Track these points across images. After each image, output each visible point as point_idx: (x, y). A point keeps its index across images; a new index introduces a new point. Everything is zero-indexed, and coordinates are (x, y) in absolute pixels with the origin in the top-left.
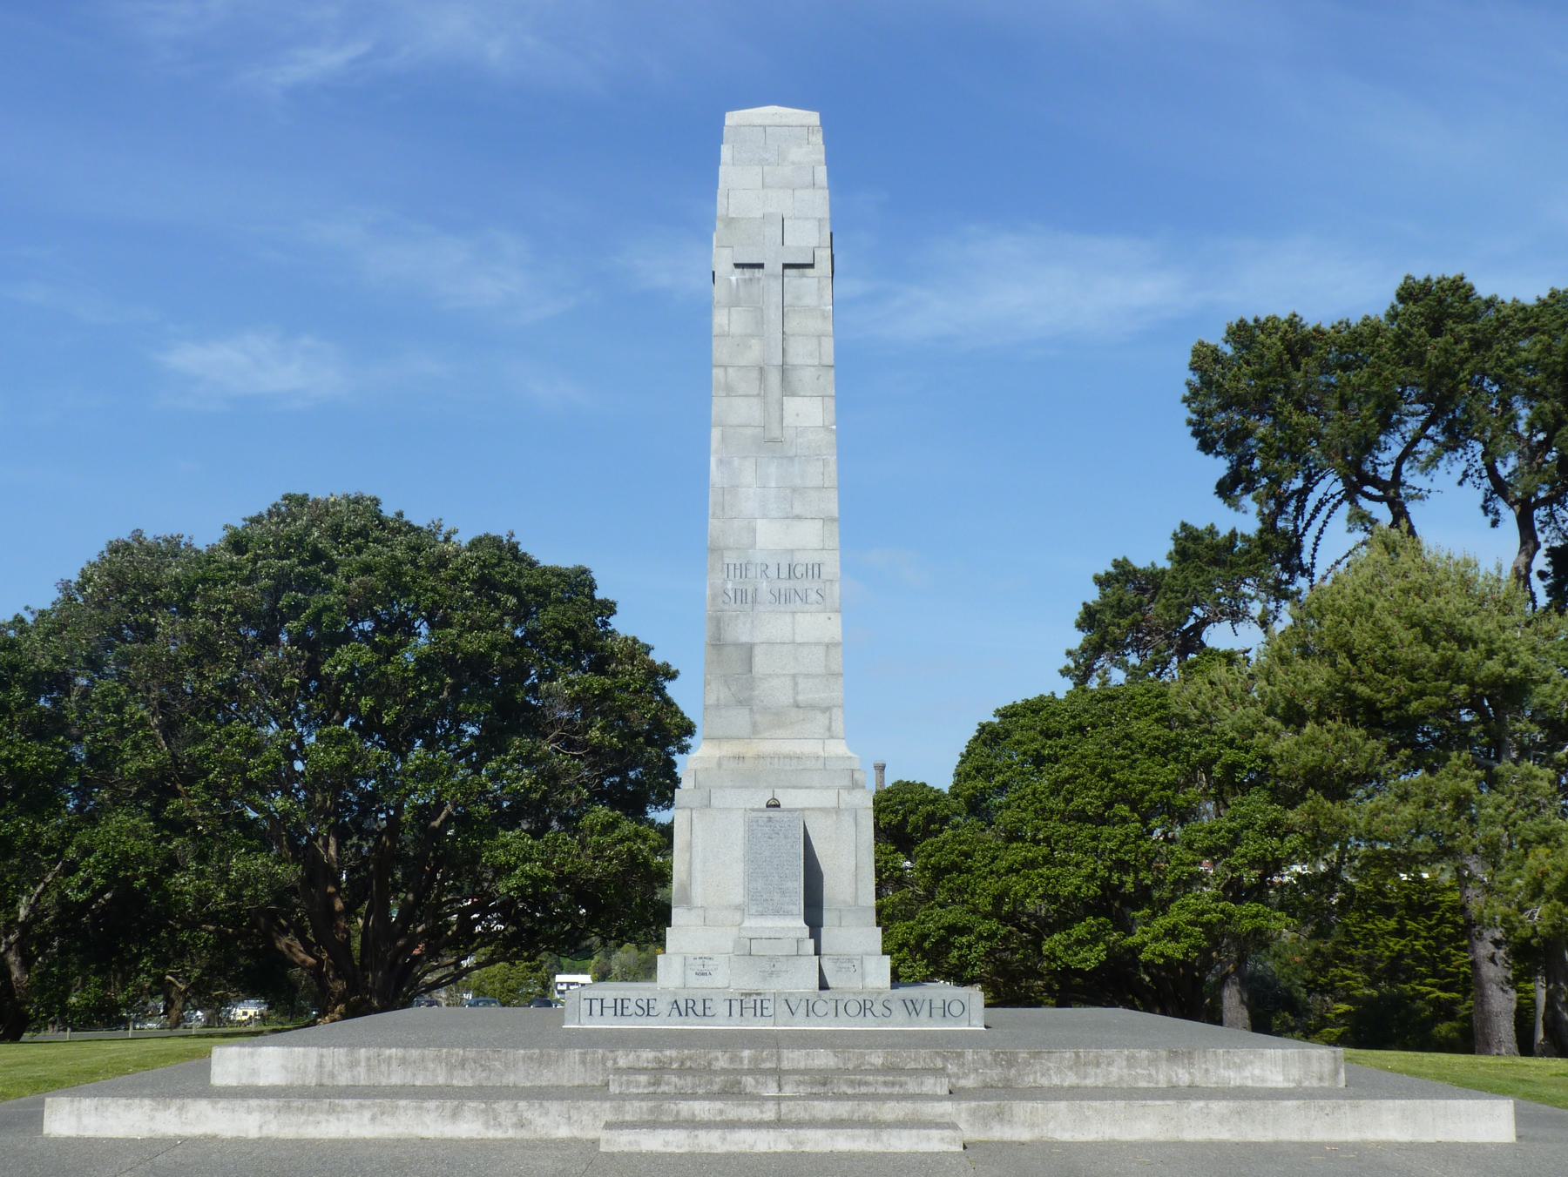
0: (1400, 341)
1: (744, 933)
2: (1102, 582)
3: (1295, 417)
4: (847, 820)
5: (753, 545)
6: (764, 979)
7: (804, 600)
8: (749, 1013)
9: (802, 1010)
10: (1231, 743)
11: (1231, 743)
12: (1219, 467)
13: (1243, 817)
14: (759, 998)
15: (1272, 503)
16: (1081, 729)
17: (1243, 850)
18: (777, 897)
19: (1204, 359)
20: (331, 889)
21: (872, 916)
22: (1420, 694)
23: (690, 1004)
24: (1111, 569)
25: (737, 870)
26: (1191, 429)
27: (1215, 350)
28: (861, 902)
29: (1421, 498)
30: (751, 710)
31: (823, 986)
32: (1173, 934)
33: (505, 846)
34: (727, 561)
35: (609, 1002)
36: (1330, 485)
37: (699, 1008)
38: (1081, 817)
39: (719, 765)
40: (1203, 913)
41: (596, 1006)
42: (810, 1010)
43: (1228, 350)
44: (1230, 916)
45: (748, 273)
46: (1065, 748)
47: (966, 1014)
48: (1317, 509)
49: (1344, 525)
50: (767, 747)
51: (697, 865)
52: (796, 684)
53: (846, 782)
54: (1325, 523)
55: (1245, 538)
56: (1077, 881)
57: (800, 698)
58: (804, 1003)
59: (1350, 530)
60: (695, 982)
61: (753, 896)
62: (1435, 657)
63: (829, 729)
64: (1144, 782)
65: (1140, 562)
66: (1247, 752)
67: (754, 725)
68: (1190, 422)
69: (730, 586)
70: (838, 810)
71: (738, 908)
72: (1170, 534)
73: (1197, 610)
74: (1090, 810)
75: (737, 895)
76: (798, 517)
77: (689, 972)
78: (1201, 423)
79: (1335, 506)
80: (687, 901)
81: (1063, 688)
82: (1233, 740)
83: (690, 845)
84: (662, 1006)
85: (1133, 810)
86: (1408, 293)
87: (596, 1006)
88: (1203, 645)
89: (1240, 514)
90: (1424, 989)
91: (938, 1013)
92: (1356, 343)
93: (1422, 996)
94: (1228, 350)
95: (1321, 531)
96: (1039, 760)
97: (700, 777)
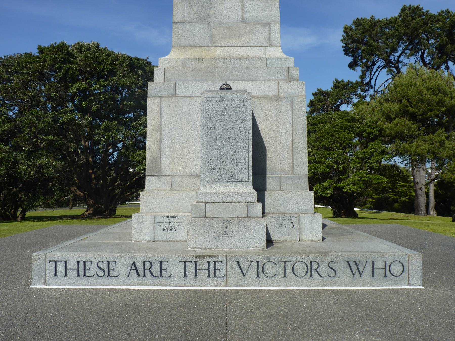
0: (403, 21)
1: (200, 198)
2: (315, 95)
3: (373, 43)
4: (285, 106)
6: (218, 239)
8: (203, 274)
9: (253, 271)
10: (369, 127)
11: (369, 127)
12: (350, 59)
13: (374, 148)
14: (212, 260)
15: (365, 68)
17: (374, 158)
18: (229, 166)
19: (347, 30)
20: (91, 171)
21: (305, 182)
22: (431, 110)
23: (148, 266)
24: (317, 91)
25: (197, 146)
26: (343, 49)
27: (350, 27)
28: (297, 171)
30: (209, 24)
31: (270, 242)
32: (354, 184)
33: (138, 155)
35: (72, 264)
36: (381, 63)
37: (156, 270)
38: (324, 148)
39: (184, 64)
40: (363, 177)
41: (61, 268)
42: (260, 271)
43: (353, 27)
44: (370, 179)
47: (405, 273)
48: (377, 70)
49: (386, 73)
50: (221, 52)
51: (166, 141)
53: (284, 76)
54: (379, 74)
55: (352, 83)
56: (324, 168)
57: (247, 15)
58: (254, 265)
59: (387, 74)
60: (162, 236)
61: (208, 166)
62: (437, 99)
63: (269, 39)
65: (324, 89)
66: (374, 129)
67: (212, 36)
68: (343, 47)
70: (277, 98)
71: (198, 176)
73: (340, 101)
74: (327, 146)
75: (197, 166)
77: (158, 228)
78: (345, 47)
79: (381, 69)
80: (158, 171)
81: (359, 80)
82: (369, 126)
83: (160, 126)
84: (121, 267)
85: (341, 146)
86: (404, 10)
87: (61, 268)
88: (340, 110)
89: (355, 72)
90: (391, 196)
91: (379, 273)
92: (390, 23)
93: (390, 197)
94: (353, 27)
95: (377, 76)
97: (168, 74)
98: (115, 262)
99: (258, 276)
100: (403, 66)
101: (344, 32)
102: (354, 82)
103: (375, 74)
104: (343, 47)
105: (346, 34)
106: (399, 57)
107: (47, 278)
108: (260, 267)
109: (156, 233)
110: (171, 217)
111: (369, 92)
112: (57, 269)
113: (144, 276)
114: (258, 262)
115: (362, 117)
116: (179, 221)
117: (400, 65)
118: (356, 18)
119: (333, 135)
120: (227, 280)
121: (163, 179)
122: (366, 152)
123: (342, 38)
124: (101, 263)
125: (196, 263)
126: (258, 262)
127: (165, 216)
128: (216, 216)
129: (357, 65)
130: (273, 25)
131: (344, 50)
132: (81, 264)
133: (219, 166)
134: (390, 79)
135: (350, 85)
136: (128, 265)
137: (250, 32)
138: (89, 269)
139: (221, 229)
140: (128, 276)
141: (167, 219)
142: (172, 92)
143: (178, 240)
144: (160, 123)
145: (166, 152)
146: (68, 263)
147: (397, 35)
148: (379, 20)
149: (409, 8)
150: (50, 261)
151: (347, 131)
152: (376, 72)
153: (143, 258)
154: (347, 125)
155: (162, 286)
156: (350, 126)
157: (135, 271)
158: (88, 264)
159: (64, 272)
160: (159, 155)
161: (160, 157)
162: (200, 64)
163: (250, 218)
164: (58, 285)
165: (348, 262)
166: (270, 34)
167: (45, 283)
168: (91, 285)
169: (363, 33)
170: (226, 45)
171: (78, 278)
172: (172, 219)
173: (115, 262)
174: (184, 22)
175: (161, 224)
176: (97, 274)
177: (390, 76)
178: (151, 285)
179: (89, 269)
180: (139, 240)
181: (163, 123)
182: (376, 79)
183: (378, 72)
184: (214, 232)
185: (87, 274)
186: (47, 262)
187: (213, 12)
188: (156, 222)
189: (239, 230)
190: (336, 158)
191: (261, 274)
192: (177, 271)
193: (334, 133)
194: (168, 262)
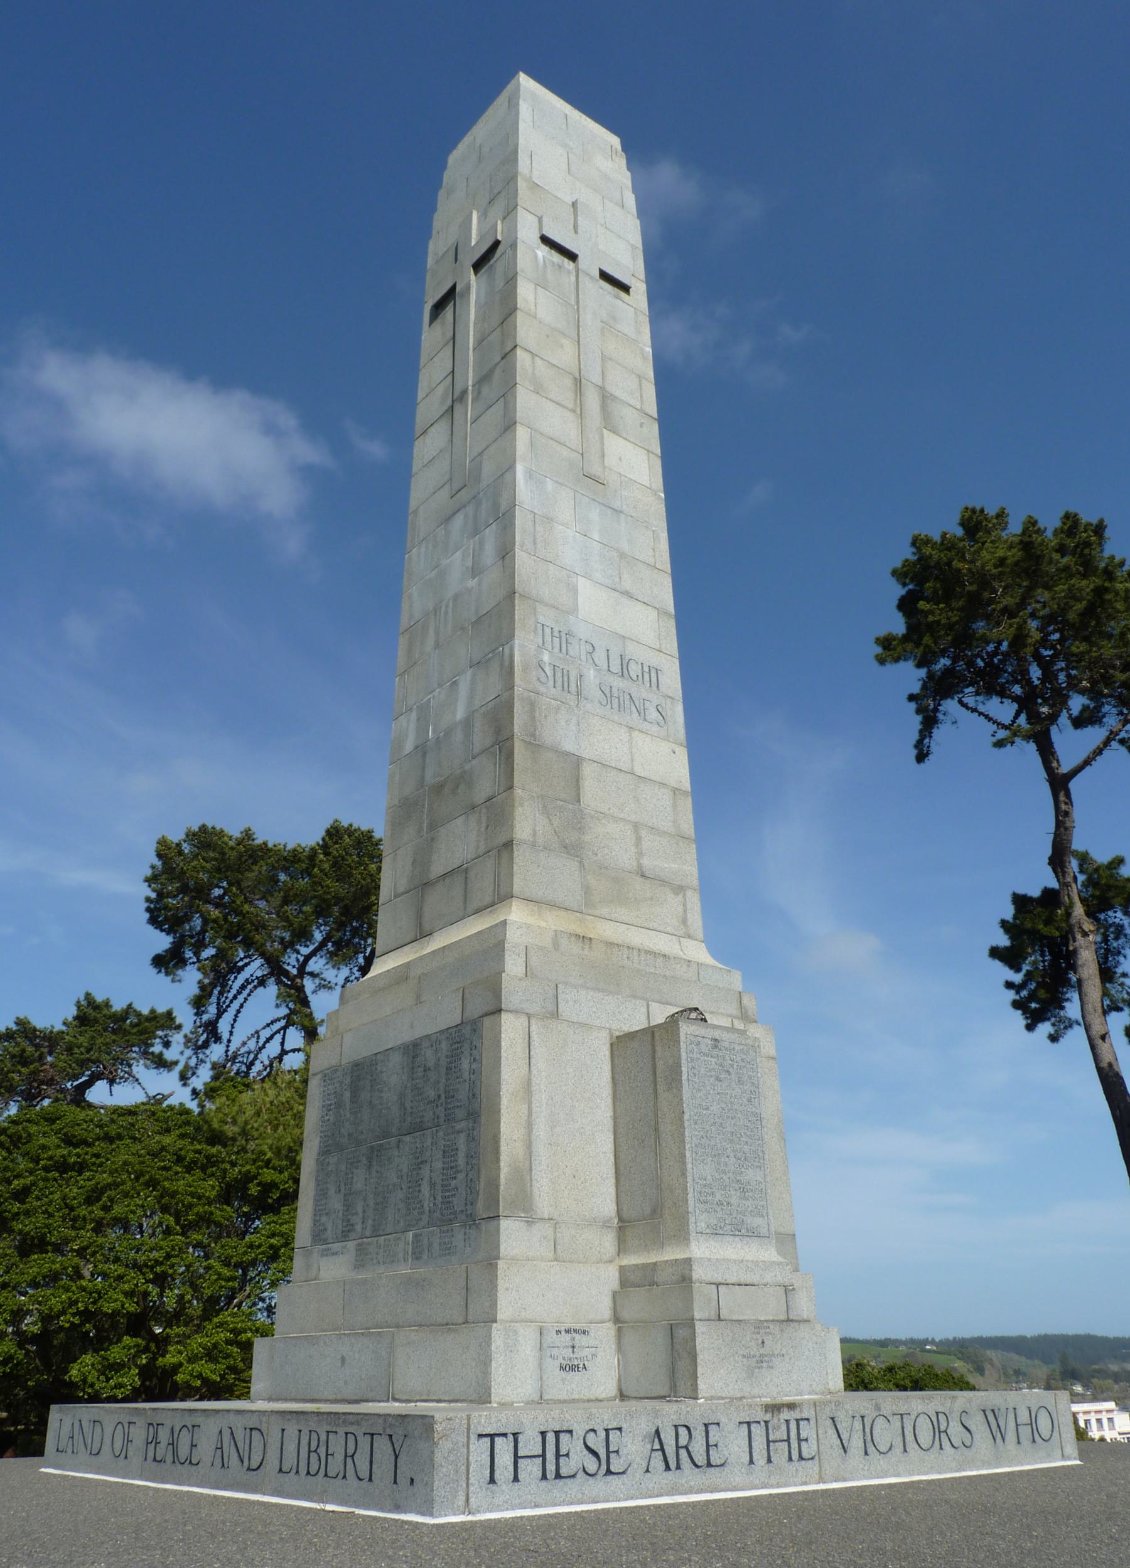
5: (574, 610)
7: (642, 712)
12: (163, 942)
13: (282, 1235)
16: (109, 1139)
19: (165, 850)
29: (330, 988)
34: (541, 619)
35: (530, 1445)
39: (556, 945)
43: (186, 848)
45: (556, 257)
46: (97, 1156)
48: (243, 987)
51: (541, 1131)
52: (639, 840)
54: (246, 999)
55: (138, 1014)
59: (277, 1006)
64: (192, 1195)
66: (281, 1172)
67: (587, 890)
68: (148, 900)
69: (546, 657)
72: (75, 1001)
76: (627, 594)
80: (525, 1207)
82: (269, 1161)
83: (528, 1087)
85: (177, 1223)
86: (335, 833)
92: (292, 860)
95: (242, 1006)
96: (63, 1167)
97: (534, 961)
98: (620, 1429)
99: (866, 1453)
100: (320, 987)
101: (159, 856)
102: (145, 1012)
103: (235, 997)
104: (148, 900)
105: (164, 863)
106: (308, 958)
107: (471, 1488)
108: (868, 1430)
109: (545, 1377)
110: (575, 1331)
111: (208, 1052)
112: (496, 1460)
113: (678, 1467)
114: (863, 1417)
115: (244, 1133)
116: (592, 1343)
117: (309, 984)
118: (200, 824)
119: (153, 1183)
120: (820, 1466)
121: (537, 1226)
122: (259, 1246)
123: (149, 872)
124: (592, 1434)
125: (766, 1422)
126: (863, 1417)
127: (563, 1329)
128: (735, 1317)
129: (182, 962)
130: (689, 893)
131: (148, 910)
132: (551, 1437)
133: (718, 1197)
134: (279, 1020)
135: (132, 1019)
136: (645, 1437)
137: (651, 899)
138: (567, 1455)
139: (755, 1350)
140: (647, 1471)
141: (568, 1337)
142: (551, 1007)
143: (593, 1397)
144: (529, 1080)
145: (541, 1150)
146: (521, 1437)
147: (315, 897)
148: (265, 844)
149: (350, 831)
150: (480, 1436)
151: (198, 1173)
152: (239, 992)
153: (674, 1417)
154: (199, 1152)
155: (712, 1492)
156: (208, 1157)
157: (660, 1453)
158: (564, 1438)
159: (511, 1468)
160: (527, 1164)
161: (531, 1170)
162: (586, 952)
163: (792, 1321)
164: (499, 1509)
165: (984, 1411)
166: (685, 911)
167: (467, 1508)
168: (571, 1504)
169: (219, 870)
170: (613, 916)
171: (544, 1483)
172: (577, 1336)
173: (620, 1429)
174: (534, 845)
175: (555, 1352)
176: (584, 1470)
177: (284, 1011)
178: (690, 1491)
179: (567, 1455)
180: (508, 1399)
181: (534, 1080)
182: (236, 1016)
183: (245, 993)
184: (744, 1356)
185: (564, 1471)
186: (473, 1437)
187: (587, 838)
188: (544, 1345)
189: (784, 1352)
190: (162, 1264)
191: (871, 1449)
192: (736, 1449)
193: (159, 1175)
194: (718, 1424)
